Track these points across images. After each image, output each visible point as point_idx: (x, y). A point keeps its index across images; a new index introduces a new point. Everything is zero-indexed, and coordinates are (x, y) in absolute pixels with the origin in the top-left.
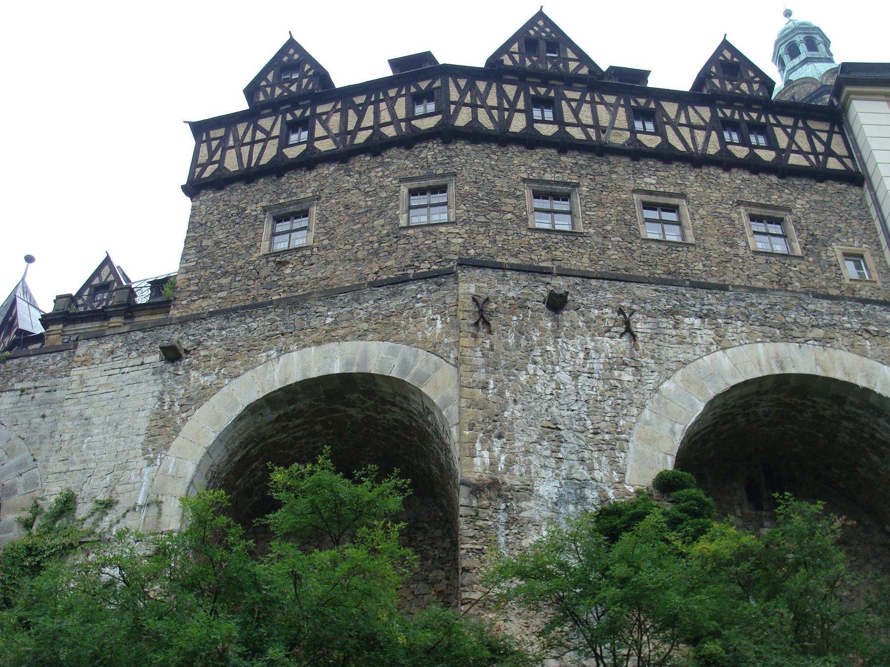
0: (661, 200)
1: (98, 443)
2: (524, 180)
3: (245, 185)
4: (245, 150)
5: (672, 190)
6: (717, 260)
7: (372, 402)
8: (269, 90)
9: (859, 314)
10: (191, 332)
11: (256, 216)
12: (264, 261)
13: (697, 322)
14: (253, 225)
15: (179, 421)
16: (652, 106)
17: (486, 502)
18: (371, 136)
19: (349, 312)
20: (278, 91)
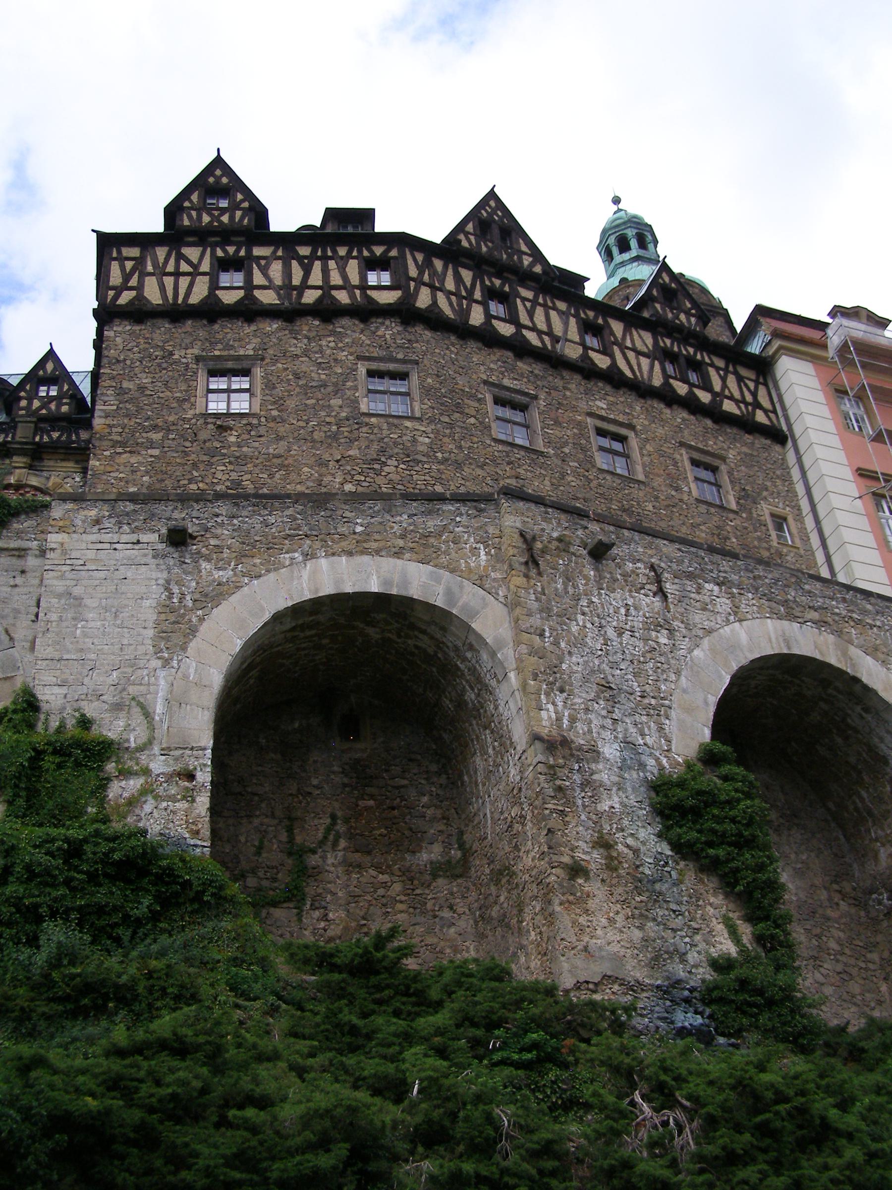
0: (612, 428)
1: (95, 631)
2: (485, 382)
3: (170, 323)
4: (169, 281)
5: (621, 418)
6: (665, 503)
7: (396, 625)
8: (194, 213)
9: (844, 600)
10: (195, 513)
11: (187, 364)
12: (201, 421)
13: (716, 588)
14: (184, 375)
15: (194, 620)
16: (600, 321)
17: (561, 761)
18: (320, 300)
19: (381, 523)
20: (206, 219)
